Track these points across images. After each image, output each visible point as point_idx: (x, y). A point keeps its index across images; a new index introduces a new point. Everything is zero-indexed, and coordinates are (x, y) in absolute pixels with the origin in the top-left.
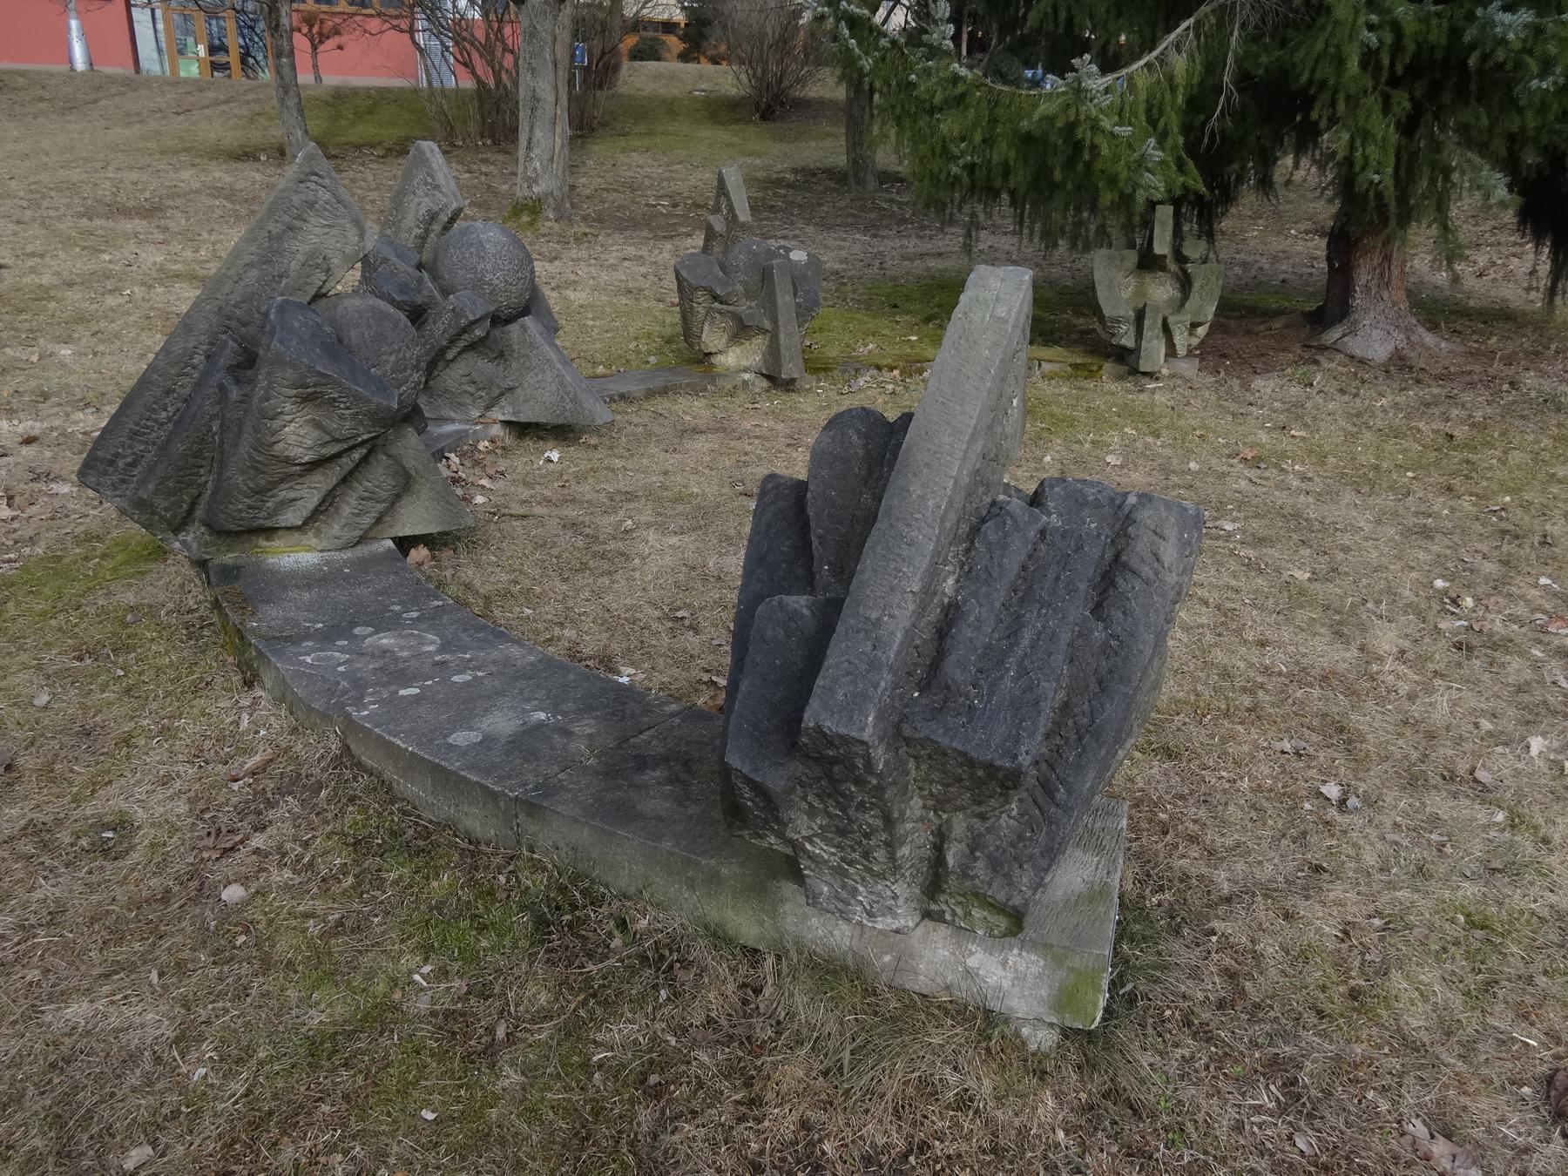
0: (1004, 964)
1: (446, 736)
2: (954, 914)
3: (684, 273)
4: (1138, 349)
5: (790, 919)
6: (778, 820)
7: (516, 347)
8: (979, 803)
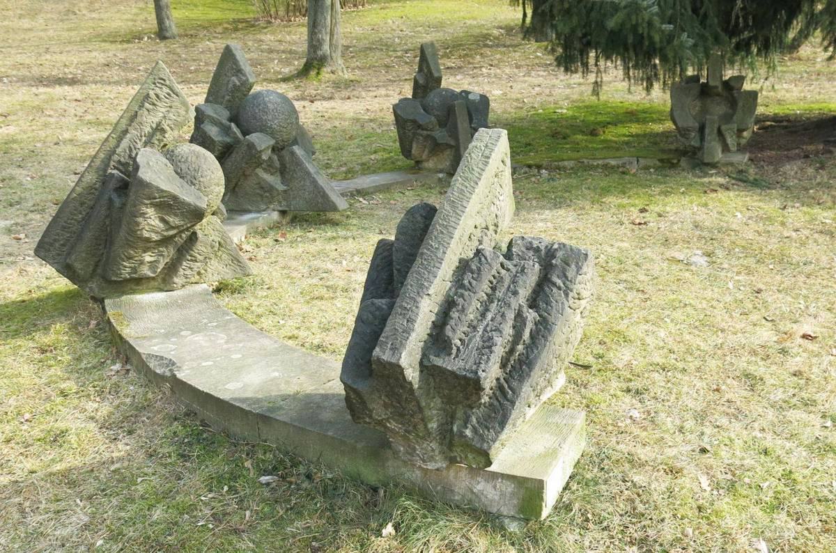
0: (495, 487)
1: (224, 385)
2: (461, 458)
3: (399, 112)
4: (701, 148)
5: (391, 469)
6: (367, 408)
7: (288, 166)
8: (468, 399)
